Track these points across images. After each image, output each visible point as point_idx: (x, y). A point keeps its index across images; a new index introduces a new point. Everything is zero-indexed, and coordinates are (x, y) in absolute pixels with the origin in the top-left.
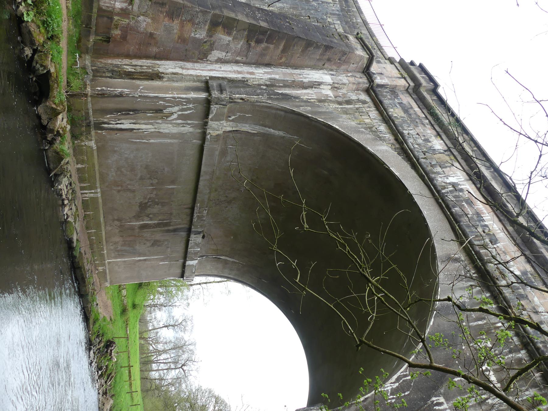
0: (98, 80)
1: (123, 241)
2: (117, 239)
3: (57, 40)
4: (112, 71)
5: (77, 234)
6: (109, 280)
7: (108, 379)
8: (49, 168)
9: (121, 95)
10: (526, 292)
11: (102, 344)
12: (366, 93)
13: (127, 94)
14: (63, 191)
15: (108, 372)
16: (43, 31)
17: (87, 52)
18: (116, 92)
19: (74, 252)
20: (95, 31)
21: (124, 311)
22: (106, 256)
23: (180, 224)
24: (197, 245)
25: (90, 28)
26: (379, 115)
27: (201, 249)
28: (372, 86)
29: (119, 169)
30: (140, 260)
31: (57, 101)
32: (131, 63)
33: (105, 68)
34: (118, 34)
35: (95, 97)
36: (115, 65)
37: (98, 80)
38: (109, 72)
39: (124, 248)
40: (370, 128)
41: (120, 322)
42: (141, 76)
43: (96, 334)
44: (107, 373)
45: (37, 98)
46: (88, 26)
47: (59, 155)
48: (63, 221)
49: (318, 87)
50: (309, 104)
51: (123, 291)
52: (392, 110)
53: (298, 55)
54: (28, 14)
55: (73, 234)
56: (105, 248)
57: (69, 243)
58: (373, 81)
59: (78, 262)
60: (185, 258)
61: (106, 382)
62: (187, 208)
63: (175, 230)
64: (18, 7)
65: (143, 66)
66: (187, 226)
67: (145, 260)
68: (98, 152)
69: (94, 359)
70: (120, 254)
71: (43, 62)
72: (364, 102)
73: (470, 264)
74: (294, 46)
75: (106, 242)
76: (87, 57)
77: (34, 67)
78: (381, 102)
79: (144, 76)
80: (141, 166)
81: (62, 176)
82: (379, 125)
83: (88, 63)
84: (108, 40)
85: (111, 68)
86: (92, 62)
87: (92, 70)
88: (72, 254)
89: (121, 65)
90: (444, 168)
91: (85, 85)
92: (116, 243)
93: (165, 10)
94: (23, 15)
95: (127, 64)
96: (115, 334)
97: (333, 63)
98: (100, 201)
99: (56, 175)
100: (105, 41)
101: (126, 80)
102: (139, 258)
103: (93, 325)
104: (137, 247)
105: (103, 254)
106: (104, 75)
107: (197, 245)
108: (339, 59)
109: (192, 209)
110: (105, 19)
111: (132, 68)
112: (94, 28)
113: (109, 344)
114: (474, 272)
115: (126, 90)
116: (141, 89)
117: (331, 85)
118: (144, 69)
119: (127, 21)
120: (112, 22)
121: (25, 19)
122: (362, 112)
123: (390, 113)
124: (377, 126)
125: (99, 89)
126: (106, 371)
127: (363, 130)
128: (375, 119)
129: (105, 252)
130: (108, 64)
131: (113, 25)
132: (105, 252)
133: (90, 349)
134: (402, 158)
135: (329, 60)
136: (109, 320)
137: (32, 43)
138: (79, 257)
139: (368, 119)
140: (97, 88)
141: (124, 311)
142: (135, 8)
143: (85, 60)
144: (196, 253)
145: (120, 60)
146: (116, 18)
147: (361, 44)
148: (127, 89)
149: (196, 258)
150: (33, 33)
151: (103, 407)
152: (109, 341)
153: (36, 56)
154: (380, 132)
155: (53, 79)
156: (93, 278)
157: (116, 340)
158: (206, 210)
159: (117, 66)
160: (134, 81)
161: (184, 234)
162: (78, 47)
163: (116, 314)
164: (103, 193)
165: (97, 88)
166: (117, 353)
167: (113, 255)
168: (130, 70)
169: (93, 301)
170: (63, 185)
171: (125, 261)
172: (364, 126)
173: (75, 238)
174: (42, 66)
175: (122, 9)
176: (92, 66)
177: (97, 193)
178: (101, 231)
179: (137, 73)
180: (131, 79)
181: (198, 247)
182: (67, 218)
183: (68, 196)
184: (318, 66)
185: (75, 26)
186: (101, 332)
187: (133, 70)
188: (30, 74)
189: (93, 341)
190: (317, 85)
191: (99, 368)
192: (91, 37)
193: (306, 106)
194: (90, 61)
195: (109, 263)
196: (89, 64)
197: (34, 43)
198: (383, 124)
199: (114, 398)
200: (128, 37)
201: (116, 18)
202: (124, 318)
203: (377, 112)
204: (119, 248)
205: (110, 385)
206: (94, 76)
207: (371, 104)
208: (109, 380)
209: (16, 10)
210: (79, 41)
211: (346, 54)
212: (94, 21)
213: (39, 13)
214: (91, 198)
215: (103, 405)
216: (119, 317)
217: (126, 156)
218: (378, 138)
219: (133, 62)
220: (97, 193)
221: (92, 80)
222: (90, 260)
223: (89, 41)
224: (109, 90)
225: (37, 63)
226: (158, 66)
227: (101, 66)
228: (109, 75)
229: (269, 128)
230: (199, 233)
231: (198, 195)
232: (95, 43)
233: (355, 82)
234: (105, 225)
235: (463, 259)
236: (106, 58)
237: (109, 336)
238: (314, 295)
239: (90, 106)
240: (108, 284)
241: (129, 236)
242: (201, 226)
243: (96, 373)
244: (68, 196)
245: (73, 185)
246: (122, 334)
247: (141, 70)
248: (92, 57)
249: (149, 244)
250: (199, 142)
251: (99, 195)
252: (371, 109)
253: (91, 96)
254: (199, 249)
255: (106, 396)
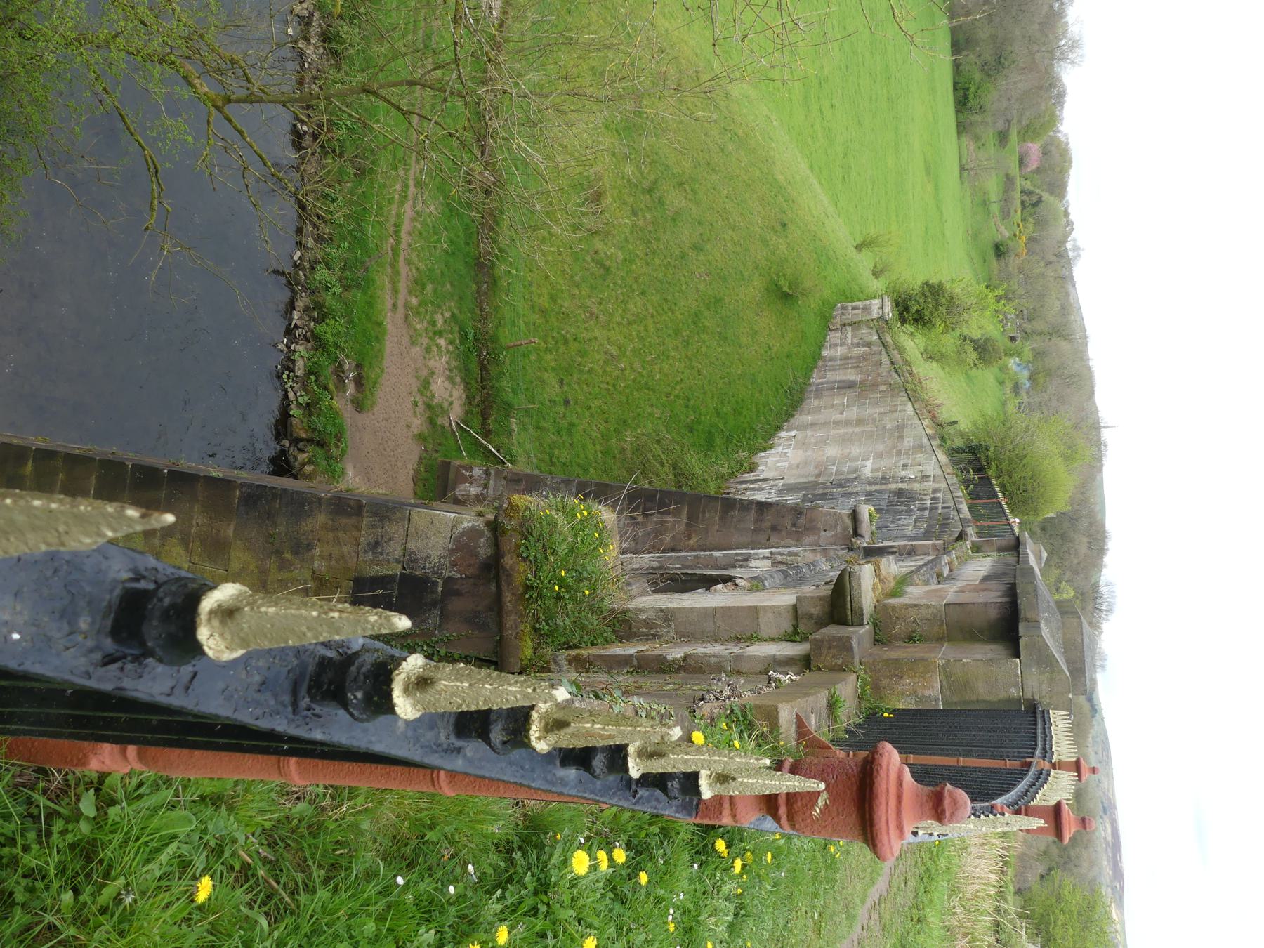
48: (567, 701)
49: (744, 564)
53: (717, 527)
74: (704, 512)
93: (523, 487)
97: (784, 533)
108: (794, 525)
117: (768, 558)
135: (774, 528)
142: (491, 491)
175: (477, 495)
184: (760, 543)
190: (742, 561)
197: (715, 660)
211: (801, 513)
238: (168, 734)
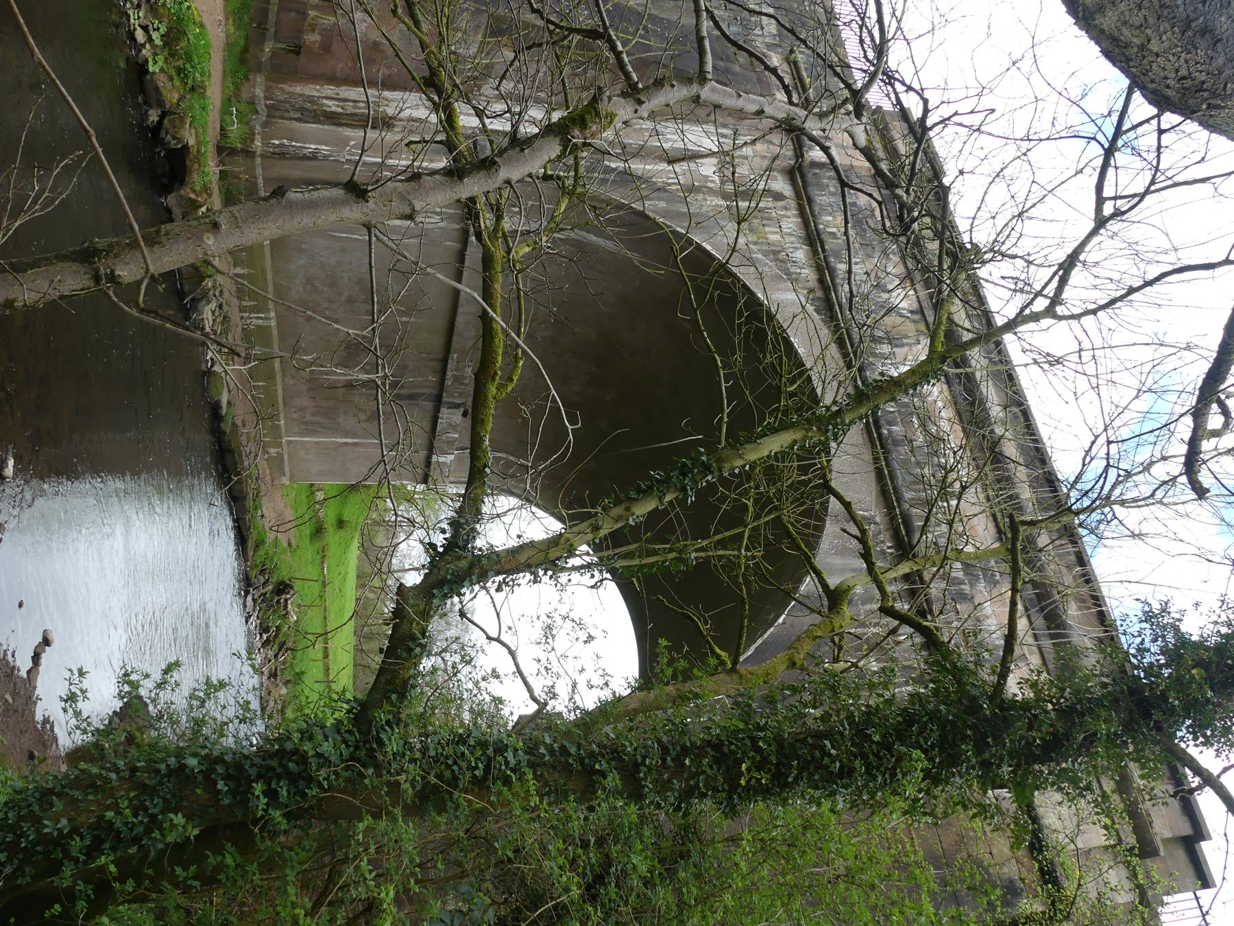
0: (275, 123)
1: (316, 406)
2: (304, 401)
3: (202, 91)
4: (302, 110)
5: (229, 391)
6: (288, 474)
7: (280, 650)
8: (183, 291)
9: (314, 157)
10: (974, 591)
11: (270, 587)
12: (787, 177)
13: (325, 156)
14: (206, 322)
15: (281, 638)
16: (177, 83)
17: (259, 68)
18: (305, 151)
19: (222, 425)
20: (275, 35)
21: (318, 531)
22: (283, 430)
23: (421, 387)
24: (454, 427)
25: (266, 29)
26: (802, 226)
27: (460, 433)
28: (800, 164)
29: (309, 280)
30: (346, 444)
31: (198, 188)
32: (338, 94)
33: (290, 103)
34: (316, 41)
35: (267, 157)
36: (309, 96)
37: (275, 123)
38: (296, 110)
39: (317, 419)
40: (776, 253)
41: (309, 551)
42: (354, 121)
43: (259, 569)
44: (277, 641)
45: (166, 182)
46: (262, 26)
47: (199, 271)
50: (665, 195)
51: (318, 494)
52: (830, 218)
54: (155, 62)
55: (221, 394)
56: (282, 415)
57: (216, 407)
58: (802, 156)
59: (229, 441)
60: (431, 449)
61: (276, 656)
62: (433, 360)
63: (411, 397)
64: (140, 51)
65: (359, 102)
66: (435, 392)
67: (355, 444)
68: (272, 248)
69: (254, 611)
70: (309, 428)
71: (176, 132)
72: (778, 197)
73: (888, 530)
75: (285, 404)
76: (259, 80)
77: (163, 139)
78: (810, 201)
79: (359, 121)
80: (349, 279)
81: (204, 302)
82: (795, 248)
83: (259, 92)
84: (297, 50)
85: (300, 103)
86: (267, 89)
87: (266, 106)
88: (219, 427)
89: (319, 97)
90: (897, 346)
91: (251, 136)
92: (302, 409)
94: (147, 61)
95: (329, 96)
96: (295, 571)
98: (275, 333)
99: (195, 301)
100: (292, 51)
101: (326, 127)
102: (344, 440)
103: (255, 552)
104: (341, 420)
105: (279, 426)
106: (286, 115)
107: (454, 427)
109: (444, 361)
110: (293, 14)
111: (338, 106)
112: (273, 30)
113: (283, 588)
114: (890, 545)
115: (324, 147)
116: (352, 147)
118: (360, 108)
119: (333, 19)
120: (304, 20)
121: (151, 69)
122: (769, 219)
123: (822, 226)
124: (791, 250)
125: (277, 142)
126: (277, 636)
127: (760, 256)
128: (790, 234)
129: (282, 422)
130: (295, 94)
131: (306, 24)
132: (282, 422)
133: (247, 593)
134: (822, 319)
136: (285, 545)
137: (160, 103)
138: (232, 431)
139: (776, 233)
140: (273, 141)
141: (318, 531)
143: (254, 86)
144: (451, 443)
145: (318, 87)
146: (312, 13)
147: (793, 74)
148: (327, 146)
149: (450, 451)
150: (162, 90)
151: (268, 698)
152: (282, 583)
153: (166, 121)
154: (793, 262)
155: (192, 156)
156: (255, 464)
157: (297, 585)
158: (469, 366)
159: (311, 100)
160: (340, 129)
161: (429, 405)
162: (242, 61)
163: (301, 536)
164: (278, 318)
165: (273, 141)
166: (299, 606)
167: (296, 429)
168: (334, 109)
169: (256, 509)
170: (207, 313)
171: (317, 443)
172: (764, 248)
173: (224, 400)
174: (174, 138)
176: (266, 98)
177: (269, 319)
178: (276, 385)
179: (347, 115)
180: (335, 124)
181: (456, 431)
182: (212, 366)
183: (216, 328)
185: (238, 28)
186: (268, 565)
187: (340, 110)
188: (156, 147)
189: (253, 580)
191: (264, 629)
192: (266, 44)
193: (659, 199)
194: (263, 87)
195: (289, 442)
196: (262, 95)
198: (804, 247)
199: (290, 686)
200: (333, 47)
201: (312, 13)
202: (318, 545)
203: (799, 220)
204: (308, 418)
205: (284, 663)
206: (269, 116)
207: (792, 204)
208: (281, 653)
209: (137, 55)
210: (246, 50)
212: (272, 18)
213: (173, 55)
214: (258, 327)
215: (269, 694)
216: (308, 542)
217: (322, 259)
218: (786, 274)
219: (341, 93)
220: (269, 319)
221: (265, 124)
222: (253, 435)
223: (262, 51)
224: (293, 146)
225: (167, 133)
226: (386, 102)
227: (281, 98)
228: (295, 116)
229: (588, 232)
230: (457, 406)
231: (454, 338)
232: (274, 54)
233: (766, 154)
234: (283, 376)
235: (878, 519)
236: (292, 81)
237: (284, 574)
239: (259, 171)
240: (285, 481)
241: (326, 399)
242: (461, 395)
243: (258, 636)
244: (216, 328)
245: (225, 308)
246: (311, 571)
247: (353, 111)
248: (267, 79)
249: (362, 417)
250: (457, 246)
251: (273, 323)
252: (789, 213)
253: (261, 155)
254: (457, 436)
255: (276, 679)
